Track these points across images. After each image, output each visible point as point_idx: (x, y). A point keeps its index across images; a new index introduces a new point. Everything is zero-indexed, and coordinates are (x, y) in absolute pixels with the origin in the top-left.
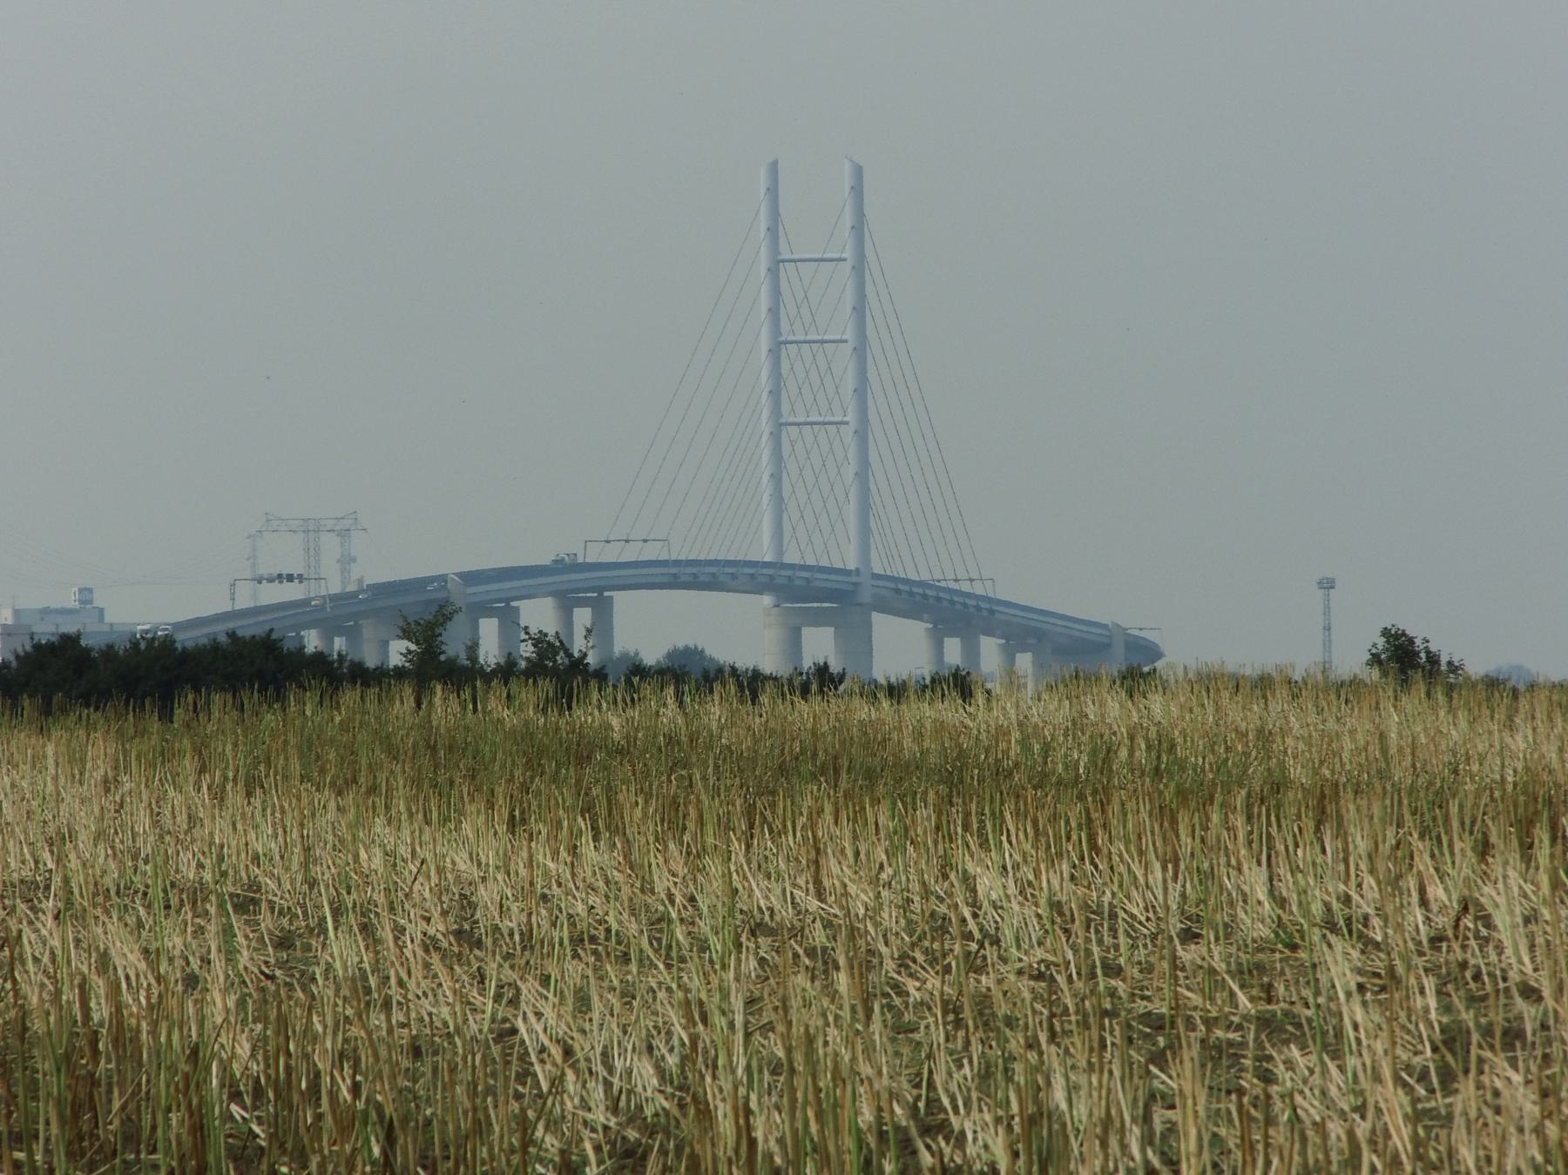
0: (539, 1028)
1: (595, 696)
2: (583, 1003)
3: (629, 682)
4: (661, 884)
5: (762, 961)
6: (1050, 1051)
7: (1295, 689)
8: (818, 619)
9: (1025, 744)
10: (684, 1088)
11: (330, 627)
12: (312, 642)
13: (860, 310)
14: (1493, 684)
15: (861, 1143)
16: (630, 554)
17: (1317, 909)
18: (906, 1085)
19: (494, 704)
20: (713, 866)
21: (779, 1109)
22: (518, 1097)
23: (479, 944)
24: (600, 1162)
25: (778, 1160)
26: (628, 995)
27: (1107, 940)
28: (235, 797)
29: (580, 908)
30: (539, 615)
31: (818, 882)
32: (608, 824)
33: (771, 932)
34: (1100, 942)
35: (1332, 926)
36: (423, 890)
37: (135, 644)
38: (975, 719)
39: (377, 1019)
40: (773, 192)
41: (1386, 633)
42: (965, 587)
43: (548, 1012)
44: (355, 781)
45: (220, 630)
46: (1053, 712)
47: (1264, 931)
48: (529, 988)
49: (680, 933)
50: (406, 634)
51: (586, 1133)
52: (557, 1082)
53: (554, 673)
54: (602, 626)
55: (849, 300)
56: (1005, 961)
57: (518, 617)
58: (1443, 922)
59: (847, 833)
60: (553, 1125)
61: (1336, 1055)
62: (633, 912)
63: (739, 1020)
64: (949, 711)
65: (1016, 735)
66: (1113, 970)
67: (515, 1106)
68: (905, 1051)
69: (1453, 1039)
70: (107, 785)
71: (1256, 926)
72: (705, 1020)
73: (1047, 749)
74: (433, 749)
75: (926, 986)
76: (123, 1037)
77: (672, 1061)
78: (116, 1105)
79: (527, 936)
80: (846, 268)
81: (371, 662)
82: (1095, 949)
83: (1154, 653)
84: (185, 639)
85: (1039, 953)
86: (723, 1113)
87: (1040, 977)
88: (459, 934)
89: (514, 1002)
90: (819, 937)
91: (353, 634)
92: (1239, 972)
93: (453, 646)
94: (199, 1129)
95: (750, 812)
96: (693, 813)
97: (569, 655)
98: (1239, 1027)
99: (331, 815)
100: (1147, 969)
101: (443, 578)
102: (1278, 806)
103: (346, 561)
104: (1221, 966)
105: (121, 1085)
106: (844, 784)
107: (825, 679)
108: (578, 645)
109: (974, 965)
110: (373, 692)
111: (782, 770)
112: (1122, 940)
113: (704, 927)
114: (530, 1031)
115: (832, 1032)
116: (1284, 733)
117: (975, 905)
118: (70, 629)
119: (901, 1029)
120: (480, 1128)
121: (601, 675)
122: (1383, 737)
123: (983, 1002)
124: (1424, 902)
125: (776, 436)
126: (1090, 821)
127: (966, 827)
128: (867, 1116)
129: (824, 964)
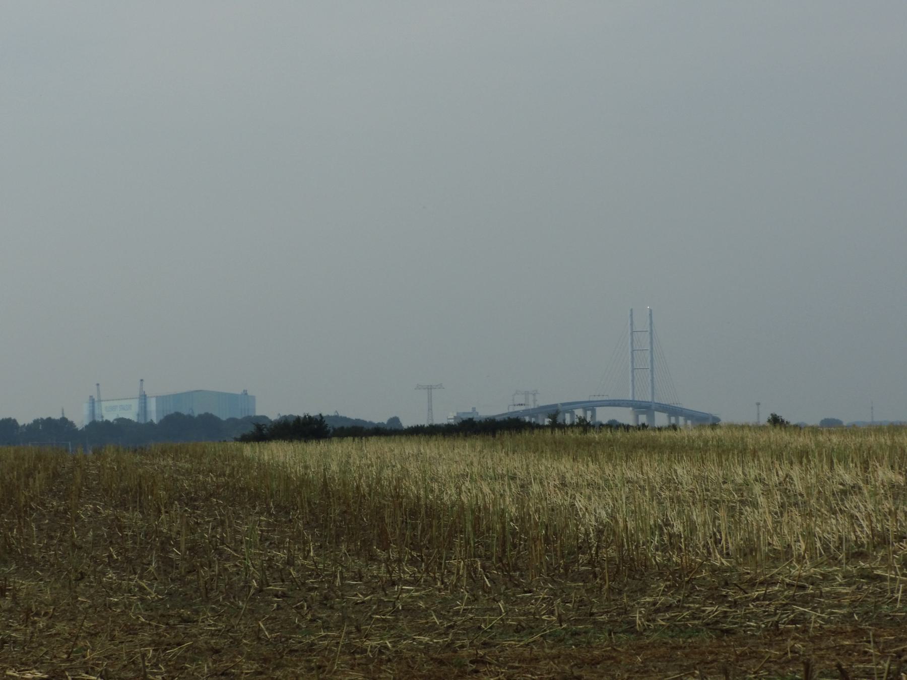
0: (580, 504)
1: (592, 430)
2: (590, 499)
3: (600, 428)
4: (607, 472)
5: (629, 489)
6: (692, 507)
7: (750, 428)
8: (643, 413)
9: (689, 441)
10: (613, 517)
11: (531, 416)
12: (527, 419)
13: (651, 343)
14: (796, 426)
15: (651, 528)
16: (600, 399)
17: (753, 476)
18: (661, 516)
19: (569, 433)
20: (618, 468)
21: (633, 521)
22: (575, 519)
23: (566, 486)
24: (594, 533)
25: (633, 532)
26: (600, 497)
27: (706, 483)
28: (511, 454)
29: (589, 478)
30: (579, 413)
31: (642, 471)
32: (595, 459)
33: (631, 482)
34: (705, 484)
35: (757, 481)
36: (554, 474)
37: (486, 420)
38: (677, 435)
39: (544, 504)
40: (631, 315)
41: (772, 415)
42: (676, 405)
43: (582, 500)
44: (538, 450)
45: (506, 417)
46: (695, 433)
47: (741, 481)
48: (578, 495)
49: (611, 482)
50: (549, 417)
51: (590, 527)
52: (584, 515)
53: (583, 426)
54: (593, 416)
55: (649, 340)
56: (683, 488)
57: (17, 423)
58: (782, 479)
59: (648, 460)
60: (583, 525)
61: (757, 509)
62: (601, 478)
63: (624, 501)
64: (671, 433)
65: (686, 438)
66: (707, 490)
67: (575, 521)
68: (661, 508)
69: (782, 506)
70: (481, 452)
71: (739, 480)
72: (617, 501)
73: (694, 441)
74: (555, 443)
75: (666, 494)
76: (486, 509)
77: (609, 511)
78: (484, 523)
79: (577, 484)
80: (648, 333)
81: (541, 423)
82: (703, 486)
83: (719, 420)
84: (498, 419)
85: (691, 486)
86: (621, 521)
87: (691, 492)
88: (562, 484)
89: (574, 499)
90: (642, 483)
91: (536, 417)
92: (735, 490)
93: (560, 420)
94: (504, 528)
95: (627, 456)
96: (614, 456)
97: (586, 421)
98: (735, 503)
99: (533, 458)
100: (715, 490)
101: (556, 405)
102: (745, 453)
103: (535, 401)
104: (731, 489)
105: (485, 518)
106: (648, 450)
107: (644, 426)
108: (588, 419)
109: (677, 489)
110: (541, 430)
111: (634, 447)
112: (709, 483)
113: (617, 481)
114: (578, 505)
115: (645, 504)
116: (747, 437)
117: (677, 476)
118: (471, 417)
119: (660, 503)
120: (567, 526)
121: (594, 426)
122: (770, 438)
123: (678, 498)
124: (778, 475)
125: (633, 372)
126: (702, 457)
127: (675, 459)
128: (652, 522)
129: (643, 489)
